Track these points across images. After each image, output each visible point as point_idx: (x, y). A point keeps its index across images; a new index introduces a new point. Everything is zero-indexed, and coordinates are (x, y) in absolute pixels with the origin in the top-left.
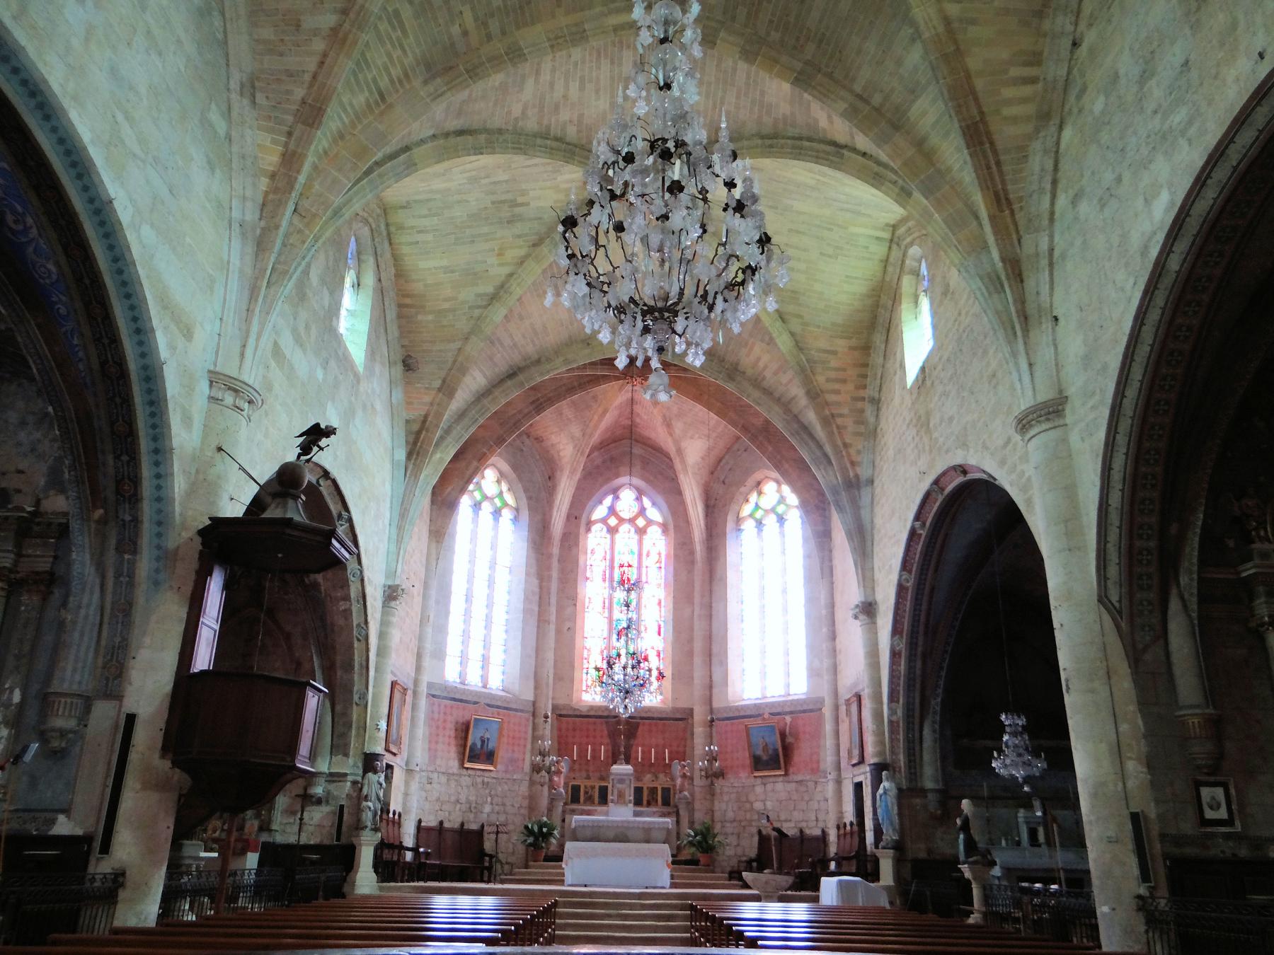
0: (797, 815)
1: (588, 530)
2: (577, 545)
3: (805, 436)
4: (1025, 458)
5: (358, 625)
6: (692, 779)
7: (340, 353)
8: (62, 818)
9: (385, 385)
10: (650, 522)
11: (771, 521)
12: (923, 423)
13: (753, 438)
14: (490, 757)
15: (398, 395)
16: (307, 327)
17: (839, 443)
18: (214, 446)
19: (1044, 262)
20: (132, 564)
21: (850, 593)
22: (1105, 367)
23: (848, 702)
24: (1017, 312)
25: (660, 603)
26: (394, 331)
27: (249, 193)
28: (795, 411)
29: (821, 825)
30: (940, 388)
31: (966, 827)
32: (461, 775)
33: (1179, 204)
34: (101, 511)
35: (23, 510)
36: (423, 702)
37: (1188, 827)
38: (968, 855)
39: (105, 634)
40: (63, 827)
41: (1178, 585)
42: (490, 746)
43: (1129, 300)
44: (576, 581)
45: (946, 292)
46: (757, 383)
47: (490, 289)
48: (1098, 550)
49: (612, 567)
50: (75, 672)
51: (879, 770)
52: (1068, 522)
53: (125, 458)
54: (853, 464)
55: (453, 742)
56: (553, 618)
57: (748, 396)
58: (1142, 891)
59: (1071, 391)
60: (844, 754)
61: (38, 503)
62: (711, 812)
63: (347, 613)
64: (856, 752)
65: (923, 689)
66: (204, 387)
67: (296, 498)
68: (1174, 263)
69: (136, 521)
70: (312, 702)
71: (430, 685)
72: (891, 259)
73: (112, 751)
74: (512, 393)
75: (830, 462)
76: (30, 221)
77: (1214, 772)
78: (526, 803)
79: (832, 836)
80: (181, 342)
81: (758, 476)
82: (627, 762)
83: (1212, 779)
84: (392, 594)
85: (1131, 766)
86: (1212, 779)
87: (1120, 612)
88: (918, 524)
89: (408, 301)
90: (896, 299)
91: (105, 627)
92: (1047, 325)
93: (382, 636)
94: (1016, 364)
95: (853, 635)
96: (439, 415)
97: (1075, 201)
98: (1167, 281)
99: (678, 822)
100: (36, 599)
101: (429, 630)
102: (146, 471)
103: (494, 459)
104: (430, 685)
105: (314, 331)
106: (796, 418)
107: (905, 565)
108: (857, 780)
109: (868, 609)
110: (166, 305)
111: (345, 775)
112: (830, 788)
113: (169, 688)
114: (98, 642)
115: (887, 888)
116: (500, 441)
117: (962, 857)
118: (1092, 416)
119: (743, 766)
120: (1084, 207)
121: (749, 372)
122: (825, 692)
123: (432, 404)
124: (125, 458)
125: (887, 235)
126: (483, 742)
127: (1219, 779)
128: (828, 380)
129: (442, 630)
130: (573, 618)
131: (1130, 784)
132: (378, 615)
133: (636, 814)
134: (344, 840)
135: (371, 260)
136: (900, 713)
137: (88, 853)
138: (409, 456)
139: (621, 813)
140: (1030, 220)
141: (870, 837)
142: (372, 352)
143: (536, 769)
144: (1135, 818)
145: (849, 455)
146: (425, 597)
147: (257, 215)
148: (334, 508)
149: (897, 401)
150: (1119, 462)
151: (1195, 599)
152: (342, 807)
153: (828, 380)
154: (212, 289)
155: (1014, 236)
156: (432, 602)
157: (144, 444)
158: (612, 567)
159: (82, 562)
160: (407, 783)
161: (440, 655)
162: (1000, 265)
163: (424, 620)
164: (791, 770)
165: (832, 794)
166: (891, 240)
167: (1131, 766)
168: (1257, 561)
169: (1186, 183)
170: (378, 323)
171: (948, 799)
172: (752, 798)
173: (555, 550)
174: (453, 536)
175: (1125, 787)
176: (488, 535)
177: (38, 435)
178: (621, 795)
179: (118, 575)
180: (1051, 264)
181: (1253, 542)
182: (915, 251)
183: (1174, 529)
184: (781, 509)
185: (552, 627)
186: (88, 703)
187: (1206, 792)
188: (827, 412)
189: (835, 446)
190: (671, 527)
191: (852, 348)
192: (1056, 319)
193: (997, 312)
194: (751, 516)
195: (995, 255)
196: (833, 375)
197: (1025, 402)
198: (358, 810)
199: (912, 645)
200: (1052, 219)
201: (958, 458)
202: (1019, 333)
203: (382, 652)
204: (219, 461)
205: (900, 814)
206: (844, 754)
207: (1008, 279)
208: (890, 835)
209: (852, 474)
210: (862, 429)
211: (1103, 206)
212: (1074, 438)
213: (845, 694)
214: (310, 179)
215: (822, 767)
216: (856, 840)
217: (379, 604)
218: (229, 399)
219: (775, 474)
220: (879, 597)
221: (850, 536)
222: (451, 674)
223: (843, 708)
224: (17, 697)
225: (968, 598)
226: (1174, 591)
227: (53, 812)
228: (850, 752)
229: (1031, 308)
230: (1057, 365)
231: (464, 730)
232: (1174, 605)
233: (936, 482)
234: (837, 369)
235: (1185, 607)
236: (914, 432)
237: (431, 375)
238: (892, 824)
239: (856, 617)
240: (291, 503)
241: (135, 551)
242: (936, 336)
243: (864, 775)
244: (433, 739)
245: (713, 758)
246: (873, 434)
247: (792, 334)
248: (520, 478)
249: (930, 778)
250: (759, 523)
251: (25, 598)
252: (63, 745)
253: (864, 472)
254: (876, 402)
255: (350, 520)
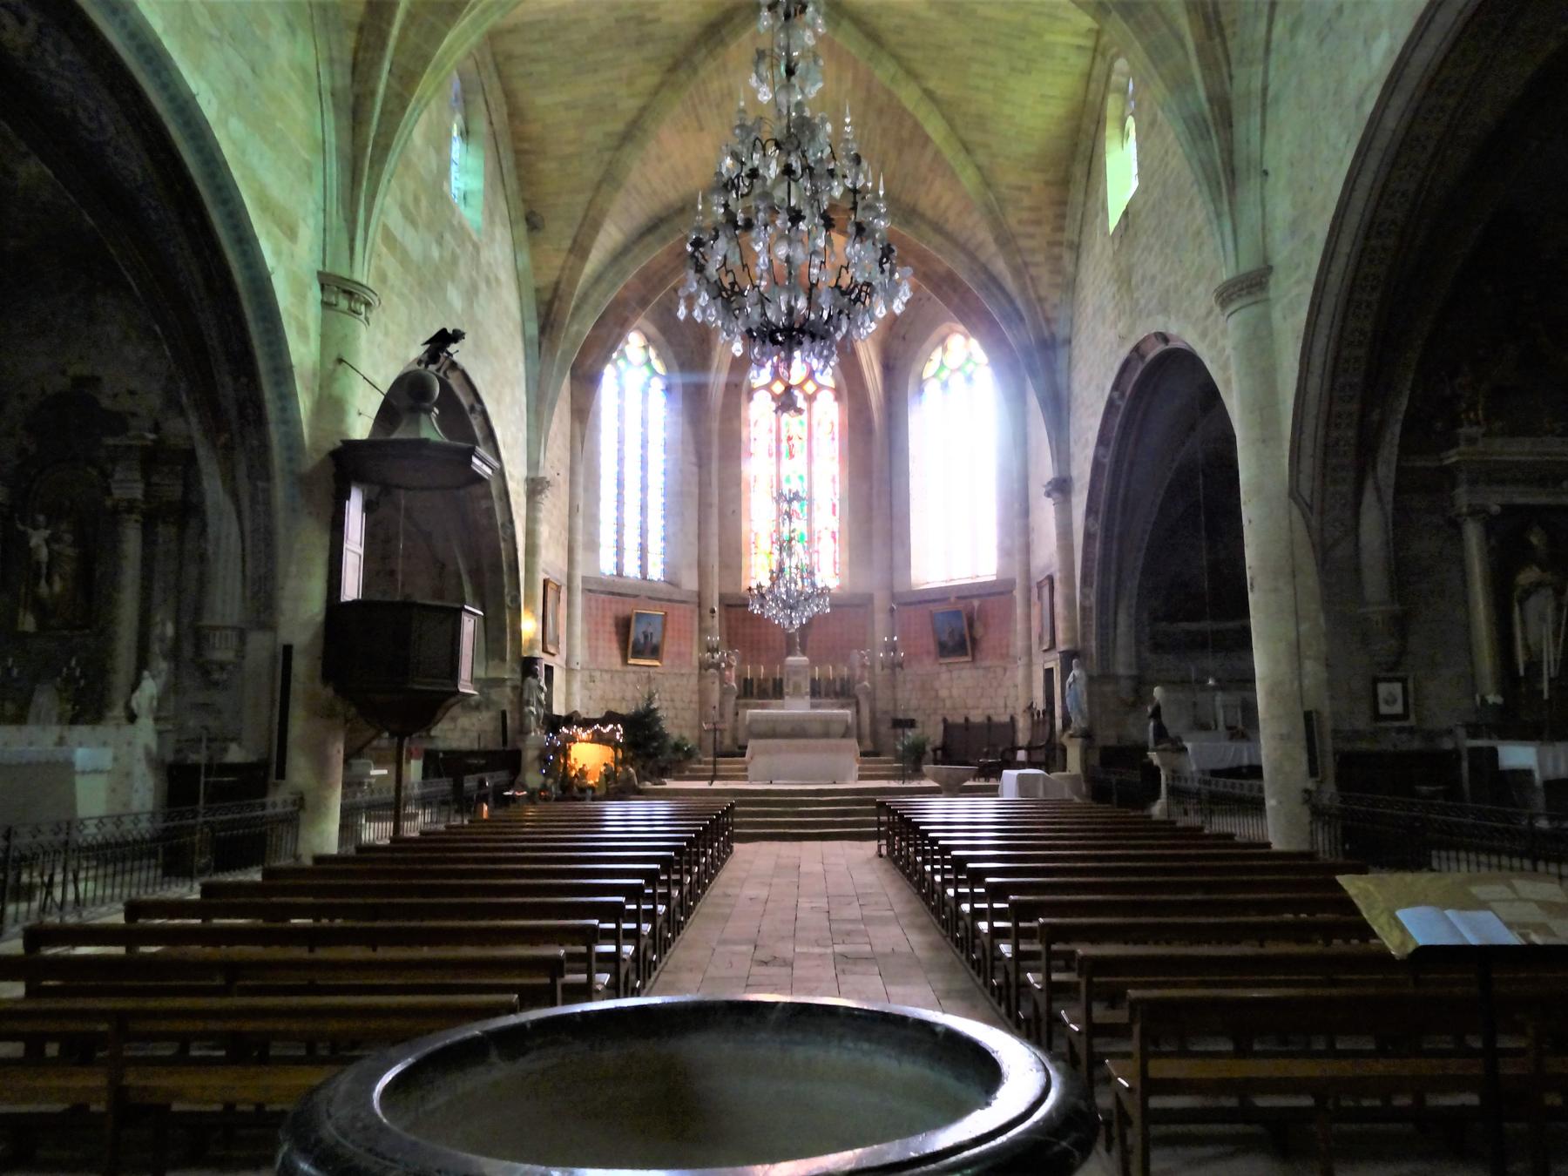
0: (985, 702)
1: (750, 398)
2: (738, 416)
3: (995, 291)
4: (1224, 333)
5: (503, 525)
6: (872, 667)
7: (455, 223)
8: (233, 747)
9: (508, 250)
10: (820, 387)
11: (957, 381)
12: (1124, 279)
13: (936, 288)
14: (655, 652)
15: (524, 259)
16: (417, 200)
17: (1033, 295)
18: (334, 356)
19: (1256, 104)
20: (267, 491)
21: (1045, 470)
22: (1312, 236)
23: (1040, 586)
24: (1223, 162)
25: (833, 480)
26: (512, 182)
27: (335, 54)
28: (983, 259)
29: (1010, 711)
30: (1144, 240)
31: (1156, 714)
32: (625, 673)
33: (1398, 50)
34: (227, 436)
35: (143, 438)
36: (579, 599)
37: (1362, 723)
38: (1157, 742)
39: (249, 565)
40: (235, 755)
41: (1375, 478)
42: (655, 640)
43: (1341, 162)
44: (739, 458)
45: (1153, 124)
46: (938, 228)
47: (619, 126)
48: (1293, 441)
49: (778, 440)
50: (226, 602)
51: (1068, 658)
52: (1264, 407)
53: (244, 380)
54: (1048, 321)
55: (614, 637)
56: (715, 500)
57: (929, 243)
58: (1310, 785)
59: (1279, 258)
60: (1035, 639)
61: (156, 428)
62: (895, 700)
63: (490, 512)
64: (1047, 638)
65: (1120, 570)
66: (315, 293)
67: (428, 411)
68: (1390, 121)
69: (265, 447)
70: (468, 626)
71: (585, 579)
72: (1095, 73)
73: (273, 679)
74: (657, 252)
75: (1022, 319)
76: (104, 118)
77: (1393, 669)
78: (695, 698)
79: (1022, 723)
80: (285, 245)
81: (943, 329)
82: (804, 653)
83: (1390, 675)
84: (535, 487)
85: (1309, 665)
86: (1390, 675)
87: (1311, 508)
88: (1116, 394)
89: (526, 146)
90: (1100, 123)
91: (248, 559)
92: (1255, 182)
93: (531, 534)
94: (1220, 226)
95: (1046, 513)
96: (573, 282)
97: (1293, 30)
98: (1382, 141)
99: (858, 712)
100: (173, 530)
101: (580, 522)
102: (269, 394)
103: (640, 321)
104: (585, 579)
105: (424, 203)
106: (985, 269)
107: (1102, 440)
108: (1048, 666)
109: (1061, 487)
110: (266, 206)
111: (504, 680)
112: (1020, 674)
113: (320, 618)
114: (243, 572)
115: (1074, 778)
116: (643, 302)
117: (1151, 745)
118: (1294, 292)
119: (929, 653)
120: (1301, 40)
121: (929, 213)
122: (1017, 574)
123: (563, 269)
124: (244, 380)
125: (1089, 43)
126: (646, 637)
127: (1399, 674)
128: (1020, 222)
129: (593, 519)
130: (737, 498)
131: (1306, 682)
132: (523, 512)
133: (813, 706)
134: (509, 748)
135: (480, 100)
136: (1093, 599)
137: (267, 775)
138: (542, 330)
139: (796, 707)
140: (1243, 50)
141: (1059, 723)
142: (490, 214)
143: (704, 666)
144: (1308, 716)
145: (1044, 311)
146: (572, 483)
147: (348, 80)
148: (465, 401)
149: (1098, 249)
150: (1320, 343)
151: (1391, 492)
152: (504, 714)
153: (1020, 222)
154: (310, 179)
155: (1225, 69)
156: (580, 491)
157: (262, 365)
158: (778, 440)
159: (213, 489)
160: (568, 683)
161: (593, 546)
162: (1206, 106)
163: (573, 510)
164: (978, 656)
165: (1018, 682)
166: (1095, 50)
167: (1309, 665)
168: (1463, 448)
169: (1405, 27)
170: (497, 176)
171: (1141, 686)
172: (937, 684)
173: (715, 425)
174: (597, 415)
175: (1301, 686)
176: (635, 390)
177: (143, 352)
178: (797, 687)
179: (253, 500)
180: (1264, 106)
181: (1461, 426)
182: (1121, 64)
183: (1375, 416)
184: (969, 368)
185: (715, 511)
186: (242, 635)
187: (1383, 689)
188: (1019, 260)
189: (1028, 302)
190: (845, 393)
191: (1047, 183)
192: (1266, 173)
193: (1201, 161)
194: (934, 376)
195: (1202, 93)
196: (1025, 215)
197: (1226, 274)
198: (522, 716)
199: (1107, 529)
200: (1267, 50)
201: (1158, 324)
202: (1224, 190)
203: (532, 550)
204: (346, 376)
205: (1090, 702)
206: (1035, 639)
207: (1215, 124)
208: (1078, 722)
209: (1046, 334)
210: (1059, 280)
211: (1322, 41)
212: (1276, 314)
213: (1038, 576)
214: (404, 29)
215: (1012, 651)
216: (1048, 727)
217: (523, 499)
218: (344, 303)
219: (961, 327)
220: (1074, 473)
221: (1044, 404)
222: (607, 566)
223: (1035, 591)
224: (170, 630)
225: (1160, 482)
226: (1369, 483)
227: (220, 740)
228: (1041, 638)
229: (1240, 162)
230: (1264, 228)
231: (623, 626)
232: (1369, 497)
233: (1137, 349)
234: (1031, 209)
235: (1380, 499)
236: (1115, 288)
237: (560, 233)
238: (1081, 711)
239: (1048, 495)
240: (423, 417)
241: (268, 478)
242: (1142, 173)
243: (1054, 662)
244: (592, 636)
245: (893, 647)
246: (1070, 286)
247: (979, 168)
248: (669, 342)
249: (1123, 664)
250: (945, 385)
251: (160, 529)
252: (225, 676)
253: (1061, 331)
254: (1076, 248)
255: (484, 413)
